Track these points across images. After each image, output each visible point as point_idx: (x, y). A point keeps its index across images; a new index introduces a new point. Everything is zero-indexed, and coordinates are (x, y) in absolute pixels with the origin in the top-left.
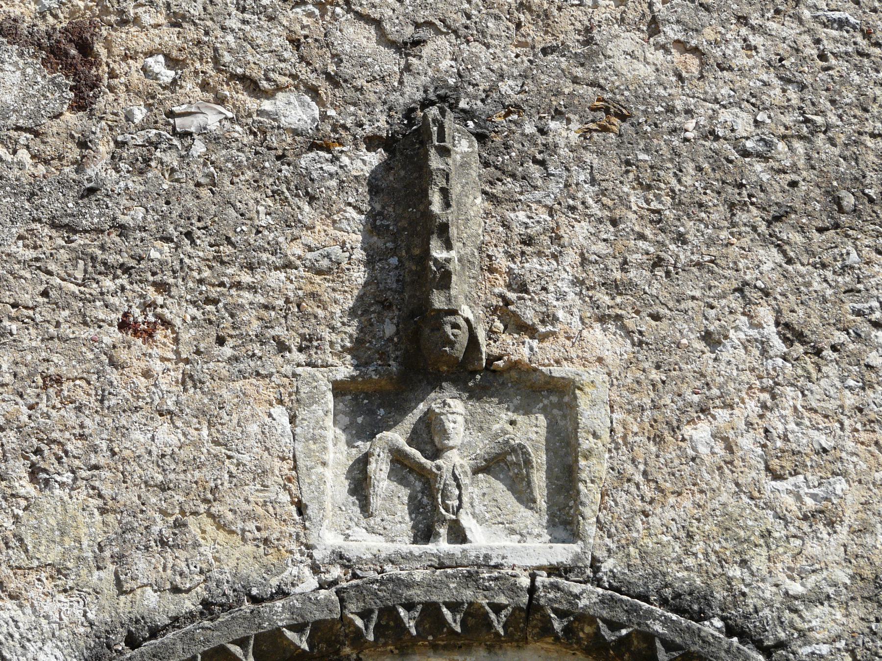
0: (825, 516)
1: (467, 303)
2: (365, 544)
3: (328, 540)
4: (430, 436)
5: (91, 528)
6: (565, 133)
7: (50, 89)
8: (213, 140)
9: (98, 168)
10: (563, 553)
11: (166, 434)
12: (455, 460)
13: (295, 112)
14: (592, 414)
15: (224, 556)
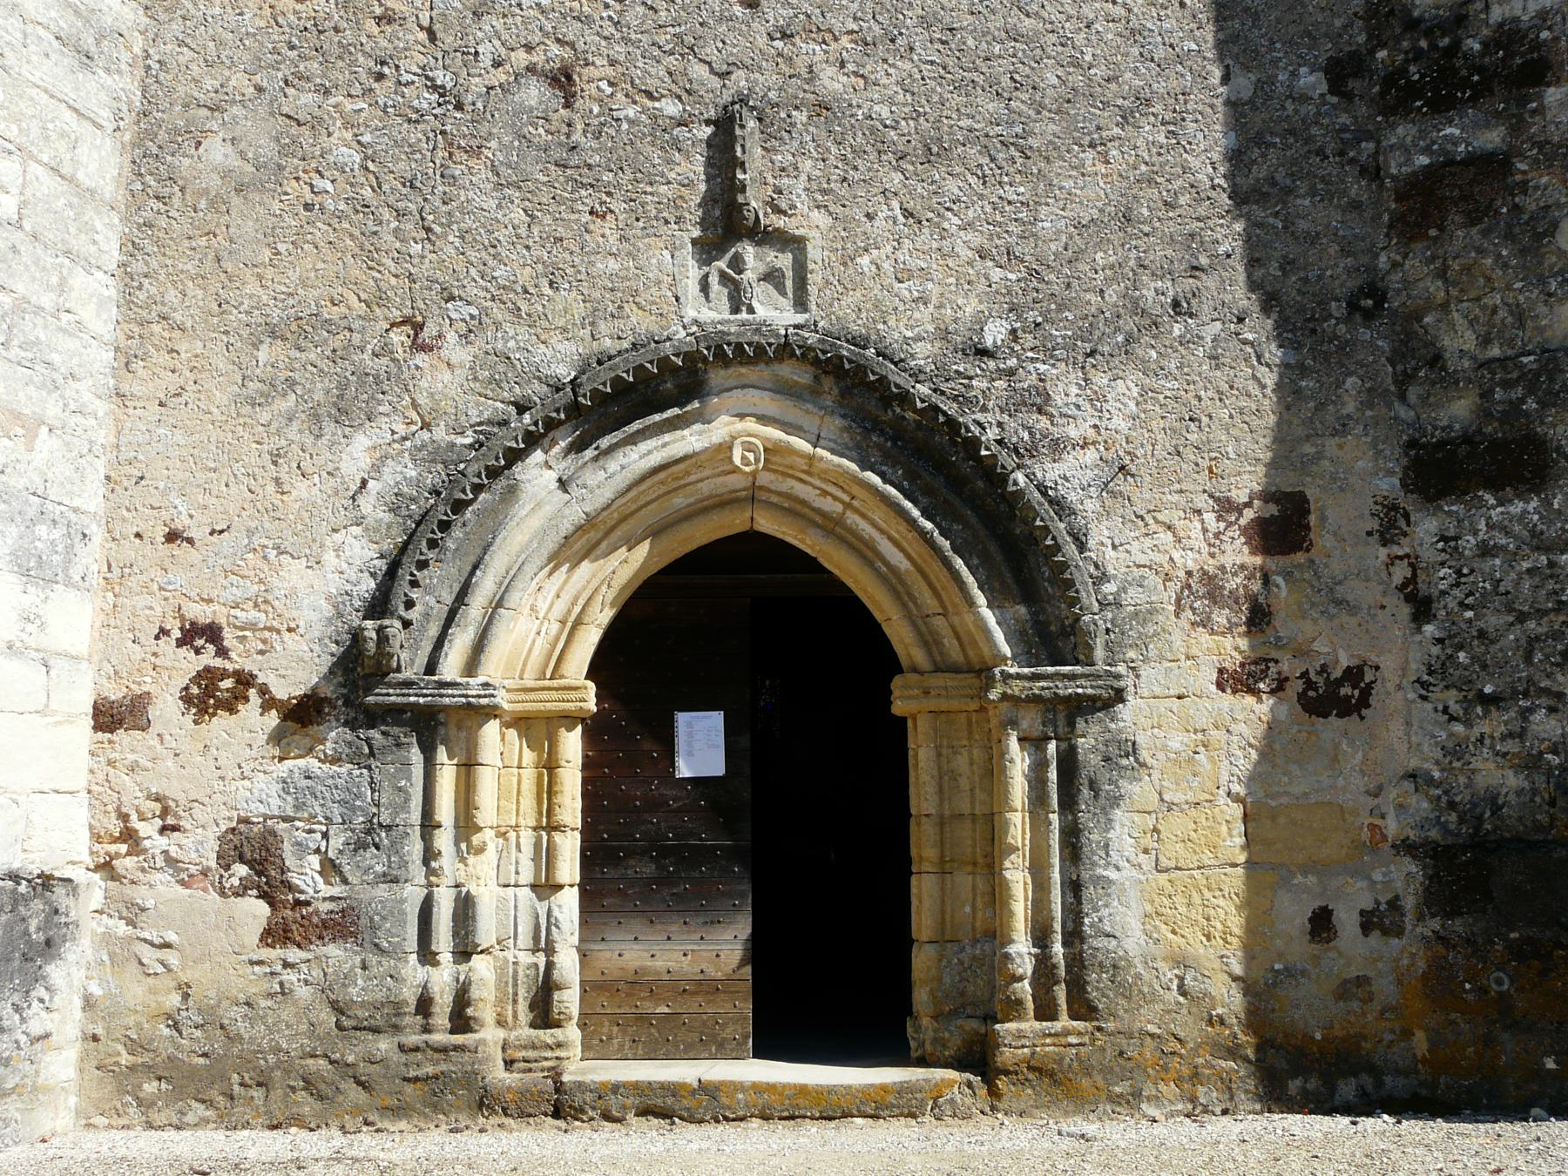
0: (923, 300)
1: (754, 200)
2: (707, 315)
3: (690, 313)
4: (737, 264)
5: (579, 310)
6: (800, 117)
7: (553, 98)
8: (631, 122)
9: (577, 137)
10: (800, 318)
11: (613, 265)
12: (749, 275)
13: (671, 108)
14: (814, 252)
15: (640, 322)
